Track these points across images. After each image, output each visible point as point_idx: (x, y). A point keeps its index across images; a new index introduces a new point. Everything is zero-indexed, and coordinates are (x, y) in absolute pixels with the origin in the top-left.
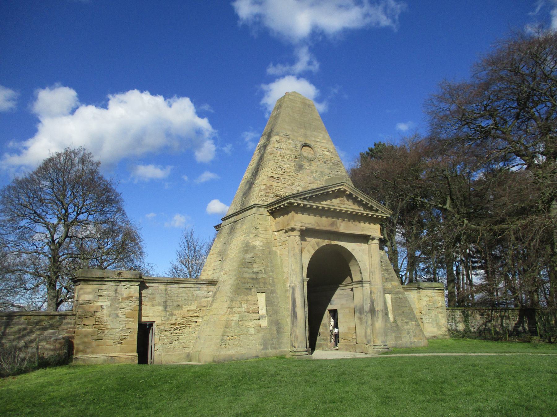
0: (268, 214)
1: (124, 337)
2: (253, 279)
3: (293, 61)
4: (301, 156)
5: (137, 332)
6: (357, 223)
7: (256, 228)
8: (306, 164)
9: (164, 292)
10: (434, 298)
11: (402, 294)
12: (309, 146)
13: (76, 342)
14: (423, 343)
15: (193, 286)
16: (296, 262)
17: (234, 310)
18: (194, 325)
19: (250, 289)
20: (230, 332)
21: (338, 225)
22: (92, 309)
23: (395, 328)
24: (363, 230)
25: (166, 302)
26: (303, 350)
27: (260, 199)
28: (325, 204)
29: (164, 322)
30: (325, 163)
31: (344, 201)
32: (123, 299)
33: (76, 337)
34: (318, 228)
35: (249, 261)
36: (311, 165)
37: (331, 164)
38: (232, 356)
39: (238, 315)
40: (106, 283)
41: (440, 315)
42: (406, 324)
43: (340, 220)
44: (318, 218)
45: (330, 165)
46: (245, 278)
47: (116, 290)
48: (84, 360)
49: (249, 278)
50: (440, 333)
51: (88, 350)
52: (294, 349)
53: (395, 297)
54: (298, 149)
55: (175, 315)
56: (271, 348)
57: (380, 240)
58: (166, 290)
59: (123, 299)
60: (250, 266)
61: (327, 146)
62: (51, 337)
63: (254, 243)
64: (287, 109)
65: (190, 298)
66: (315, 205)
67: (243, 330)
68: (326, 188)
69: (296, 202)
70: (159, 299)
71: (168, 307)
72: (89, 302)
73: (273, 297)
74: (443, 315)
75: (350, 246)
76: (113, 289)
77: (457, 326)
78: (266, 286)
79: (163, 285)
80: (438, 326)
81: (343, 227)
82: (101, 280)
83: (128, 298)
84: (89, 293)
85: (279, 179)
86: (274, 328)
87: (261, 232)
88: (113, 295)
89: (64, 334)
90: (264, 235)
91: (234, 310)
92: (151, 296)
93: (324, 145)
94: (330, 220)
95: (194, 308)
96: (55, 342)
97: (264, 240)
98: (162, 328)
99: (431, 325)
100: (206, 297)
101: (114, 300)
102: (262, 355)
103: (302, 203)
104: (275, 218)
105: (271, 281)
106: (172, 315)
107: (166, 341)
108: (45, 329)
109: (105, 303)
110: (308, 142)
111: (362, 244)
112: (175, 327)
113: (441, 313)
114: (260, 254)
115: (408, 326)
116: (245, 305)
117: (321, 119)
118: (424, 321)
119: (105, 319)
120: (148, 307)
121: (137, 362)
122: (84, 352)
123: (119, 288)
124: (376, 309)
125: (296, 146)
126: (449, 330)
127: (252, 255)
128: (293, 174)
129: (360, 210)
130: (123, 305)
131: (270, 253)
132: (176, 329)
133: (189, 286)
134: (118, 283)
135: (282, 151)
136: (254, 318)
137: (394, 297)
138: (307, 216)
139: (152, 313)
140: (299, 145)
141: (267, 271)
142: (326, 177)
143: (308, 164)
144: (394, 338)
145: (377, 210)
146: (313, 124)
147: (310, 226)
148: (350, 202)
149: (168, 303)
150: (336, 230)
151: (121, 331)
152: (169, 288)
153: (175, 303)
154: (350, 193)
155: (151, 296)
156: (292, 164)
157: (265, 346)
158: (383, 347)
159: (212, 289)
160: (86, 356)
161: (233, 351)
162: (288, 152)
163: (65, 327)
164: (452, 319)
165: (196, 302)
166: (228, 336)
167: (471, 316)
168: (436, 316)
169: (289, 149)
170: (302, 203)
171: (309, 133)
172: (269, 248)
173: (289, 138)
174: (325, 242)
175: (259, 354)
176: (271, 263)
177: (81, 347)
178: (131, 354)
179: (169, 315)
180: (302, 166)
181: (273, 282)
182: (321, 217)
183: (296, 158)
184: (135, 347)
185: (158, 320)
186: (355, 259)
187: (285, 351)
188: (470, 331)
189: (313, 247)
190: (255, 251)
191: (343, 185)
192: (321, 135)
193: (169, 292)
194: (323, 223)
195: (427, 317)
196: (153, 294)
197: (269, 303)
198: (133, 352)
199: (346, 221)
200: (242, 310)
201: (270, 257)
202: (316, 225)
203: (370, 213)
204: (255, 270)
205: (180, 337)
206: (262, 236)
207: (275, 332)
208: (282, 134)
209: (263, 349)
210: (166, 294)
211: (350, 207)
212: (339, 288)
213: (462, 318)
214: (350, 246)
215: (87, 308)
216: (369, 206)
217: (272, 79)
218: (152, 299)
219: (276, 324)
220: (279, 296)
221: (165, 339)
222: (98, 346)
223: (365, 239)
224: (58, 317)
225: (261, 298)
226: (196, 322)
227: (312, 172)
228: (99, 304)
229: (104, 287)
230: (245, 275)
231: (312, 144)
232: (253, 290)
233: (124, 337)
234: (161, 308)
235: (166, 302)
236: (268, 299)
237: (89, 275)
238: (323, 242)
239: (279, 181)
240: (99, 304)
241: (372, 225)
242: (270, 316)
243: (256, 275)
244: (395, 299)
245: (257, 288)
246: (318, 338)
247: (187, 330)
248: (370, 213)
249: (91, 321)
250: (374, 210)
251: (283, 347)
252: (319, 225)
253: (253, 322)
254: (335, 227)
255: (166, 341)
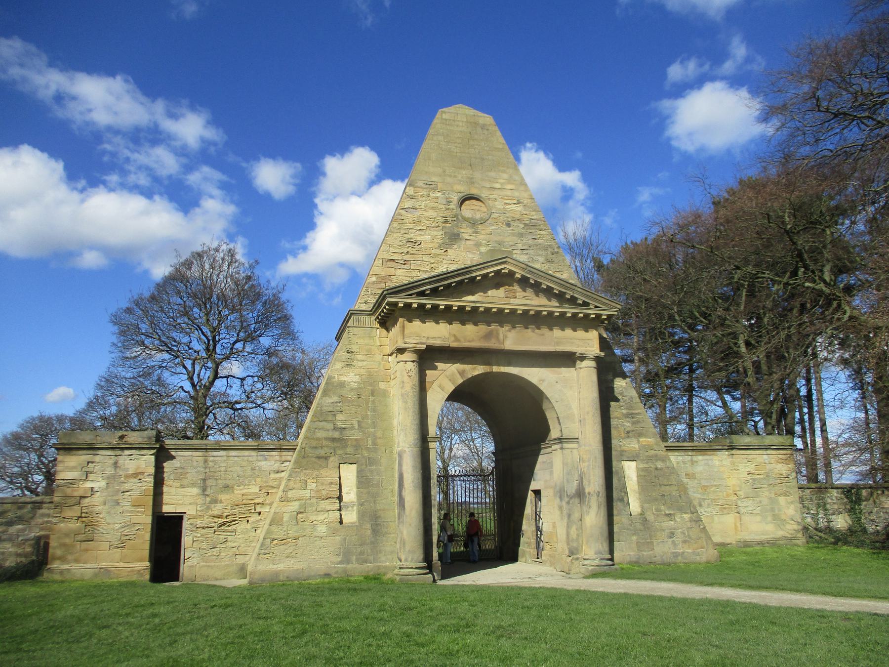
0: (378, 326)
1: (128, 537)
2: (333, 440)
3: (718, 56)
4: (457, 219)
5: (149, 530)
6: (545, 330)
7: (349, 352)
8: (466, 232)
9: (201, 464)
10: (768, 467)
11: (663, 461)
12: (477, 199)
13: (53, 543)
14: (708, 554)
15: (254, 453)
16: (405, 409)
17: (291, 494)
18: (255, 517)
19: (326, 458)
20: (278, 532)
21: (501, 337)
22: (76, 494)
23: (639, 526)
24: (558, 344)
25: (204, 480)
26: (413, 565)
27: (363, 300)
28: (469, 300)
29: (202, 513)
30: (508, 225)
31: (515, 292)
32: (128, 477)
33: (52, 537)
34: (454, 345)
35: (330, 409)
36: (477, 233)
37: (522, 226)
38: (277, 574)
39: (297, 503)
40: (100, 452)
41: (782, 500)
42: (666, 519)
43: (506, 327)
44: (456, 327)
45: (519, 227)
46: (318, 439)
47: (116, 463)
48: (62, 572)
49: (326, 439)
50: (780, 533)
51: (70, 557)
52: (399, 563)
53: (645, 466)
54: (452, 206)
55: (221, 502)
56: (357, 560)
57: (597, 359)
58: (206, 461)
59: (128, 477)
60: (330, 418)
61: (516, 194)
62: (18, 536)
63: (343, 378)
64: (435, 138)
65: (249, 473)
66: (442, 303)
67: (304, 530)
68: (467, 270)
69: (401, 300)
70: (193, 475)
71: (209, 489)
72: (73, 482)
73: (371, 471)
74: (790, 499)
75: (534, 375)
76: (112, 461)
77: (830, 521)
78: (359, 452)
79: (200, 454)
80: (777, 519)
81: (511, 339)
82: (91, 448)
83: (136, 475)
84: (72, 469)
85: (405, 262)
86: (368, 526)
87: (359, 357)
88: (110, 470)
89: (35, 533)
90: (364, 363)
91: (291, 494)
92: (180, 471)
93: (509, 193)
94: (483, 328)
95: (255, 489)
96: (24, 544)
97: (363, 371)
98: (198, 522)
99: (758, 518)
100: (278, 472)
101: (111, 480)
102: (336, 573)
103: (415, 302)
104: (388, 330)
105: (370, 442)
106: (215, 501)
107: (204, 545)
108: (10, 524)
109: (97, 483)
110: (474, 191)
111: (563, 369)
112: (220, 521)
113: (785, 494)
114: (352, 396)
115: (672, 523)
116: (314, 486)
117: (506, 147)
118: (743, 510)
119: (97, 509)
120: (173, 490)
121: (148, 577)
122: (63, 559)
123: (121, 460)
124: (587, 491)
125: (449, 202)
126: (805, 529)
127: (336, 399)
128: (438, 251)
129: (553, 306)
130: (127, 486)
131: (372, 394)
132: (224, 524)
133: (247, 453)
134: (120, 453)
135: (419, 213)
136: (329, 507)
137: (642, 466)
138: (419, 323)
139: (180, 498)
140: (455, 198)
141: (363, 425)
142: (483, 249)
143: (470, 230)
144: (634, 545)
145: (586, 304)
146: (490, 157)
147: (438, 342)
148: (530, 292)
149: (209, 483)
150: (501, 347)
151: (122, 527)
152: (212, 458)
153: (221, 483)
154: (522, 276)
155: (180, 471)
156: (436, 233)
157: (346, 555)
158: (597, 562)
159: (289, 458)
160: (65, 566)
161: (284, 564)
162: (431, 213)
163: (40, 521)
164: (818, 506)
165: (258, 480)
166: (274, 539)
167: (867, 500)
168: (772, 501)
169: (433, 208)
170: (415, 302)
171: (477, 175)
172: (371, 385)
173: (435, 190)
174: (479, 370)
175: (332, 572)
176: (374, 410)
177: (59, 552)
178: (138, 564)
179: (210, 503)
180: (458, 235)
181: (374, 443)
182: (463, 324)
183: (446, 222)
184: (146, 553)
185: (190, 510)
186: (547, 398)
187: (386, 567)
188: (864, 531)
189: (452, 381)
190: (343, 392)
191: (505, 262)
192: (505, 176)
193: (211, 464)
194: (468, 335)
195: (749, 502)
196: (183, 468)
197: (363, 482)
198: (141, 560)
199: (519, 328)
200: (307, 493)
201: (373, 402)
202: (453, 339)
203: (569, 311)
204: (339, 424)
205: (229, 538)
206: (360, 364)
207: (369, 532)
208: (420, 184)
209: (340, 563)
210: (206, 468)
211: (528, 302)
212: (542, 452)
213: (845, 504)
214: (534, 375)
215: (69, 491)
216: (568, 296)
217: (681, 90)
218: (180, 476)
219: (374, 520)
220: (382, 469)
221: (203, 542)
222: (86, 550)
223: (568, 359)
224: (29, 506)
225: (349, 474)
226: (260, 513)
227: (478, 245)
228: (88, 485)
229: (97, 459)
230: (319, 434)
231: (484, 194)
232: (332, 459)
233: (128, 537)
234: (195, 491)
235: (204, 480)
236: (360, 473)
237: (73, 441)
238: (474, 369)
239: (405, 267)
240: (88, 485)
241: (580, 333)
242: (362, 505)
243: (341, 433)
244: (644, 470)
245: (340, 455)
246: (522, 539)
247: (242, 526)
248: (569, 311)
249: (75, 512)
250: (579, 305)
251: (383, 559)
252: (457, 340)
253: (326, 515)
254: (493, 341)
255: (204, 545)
